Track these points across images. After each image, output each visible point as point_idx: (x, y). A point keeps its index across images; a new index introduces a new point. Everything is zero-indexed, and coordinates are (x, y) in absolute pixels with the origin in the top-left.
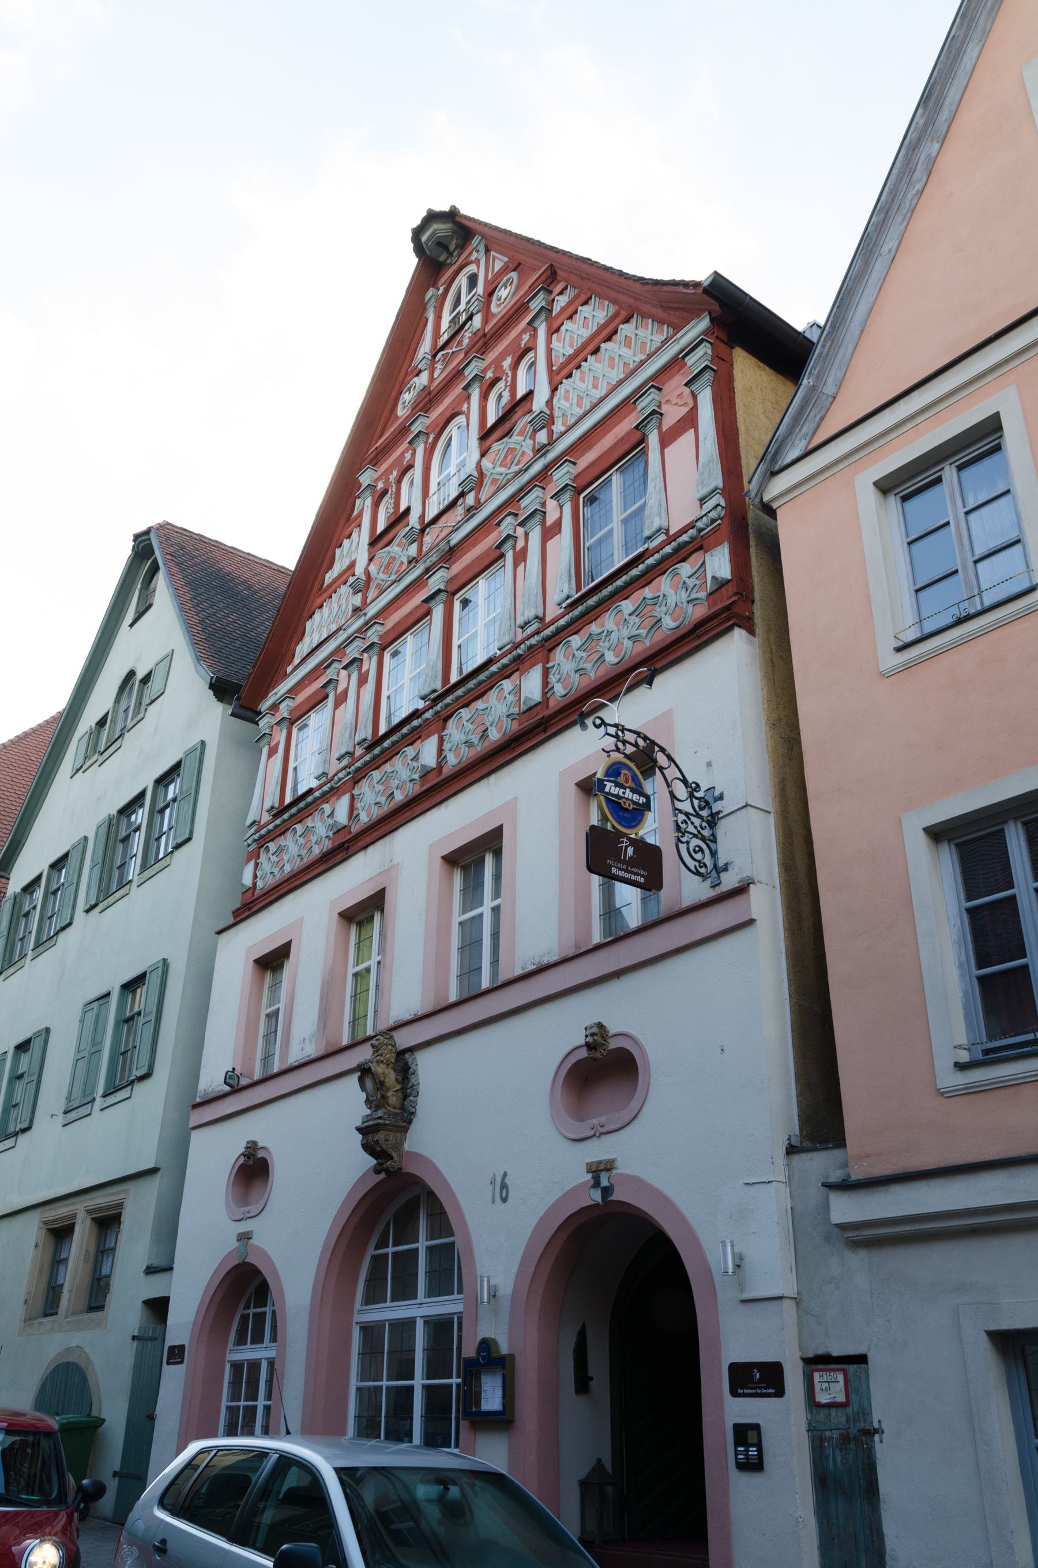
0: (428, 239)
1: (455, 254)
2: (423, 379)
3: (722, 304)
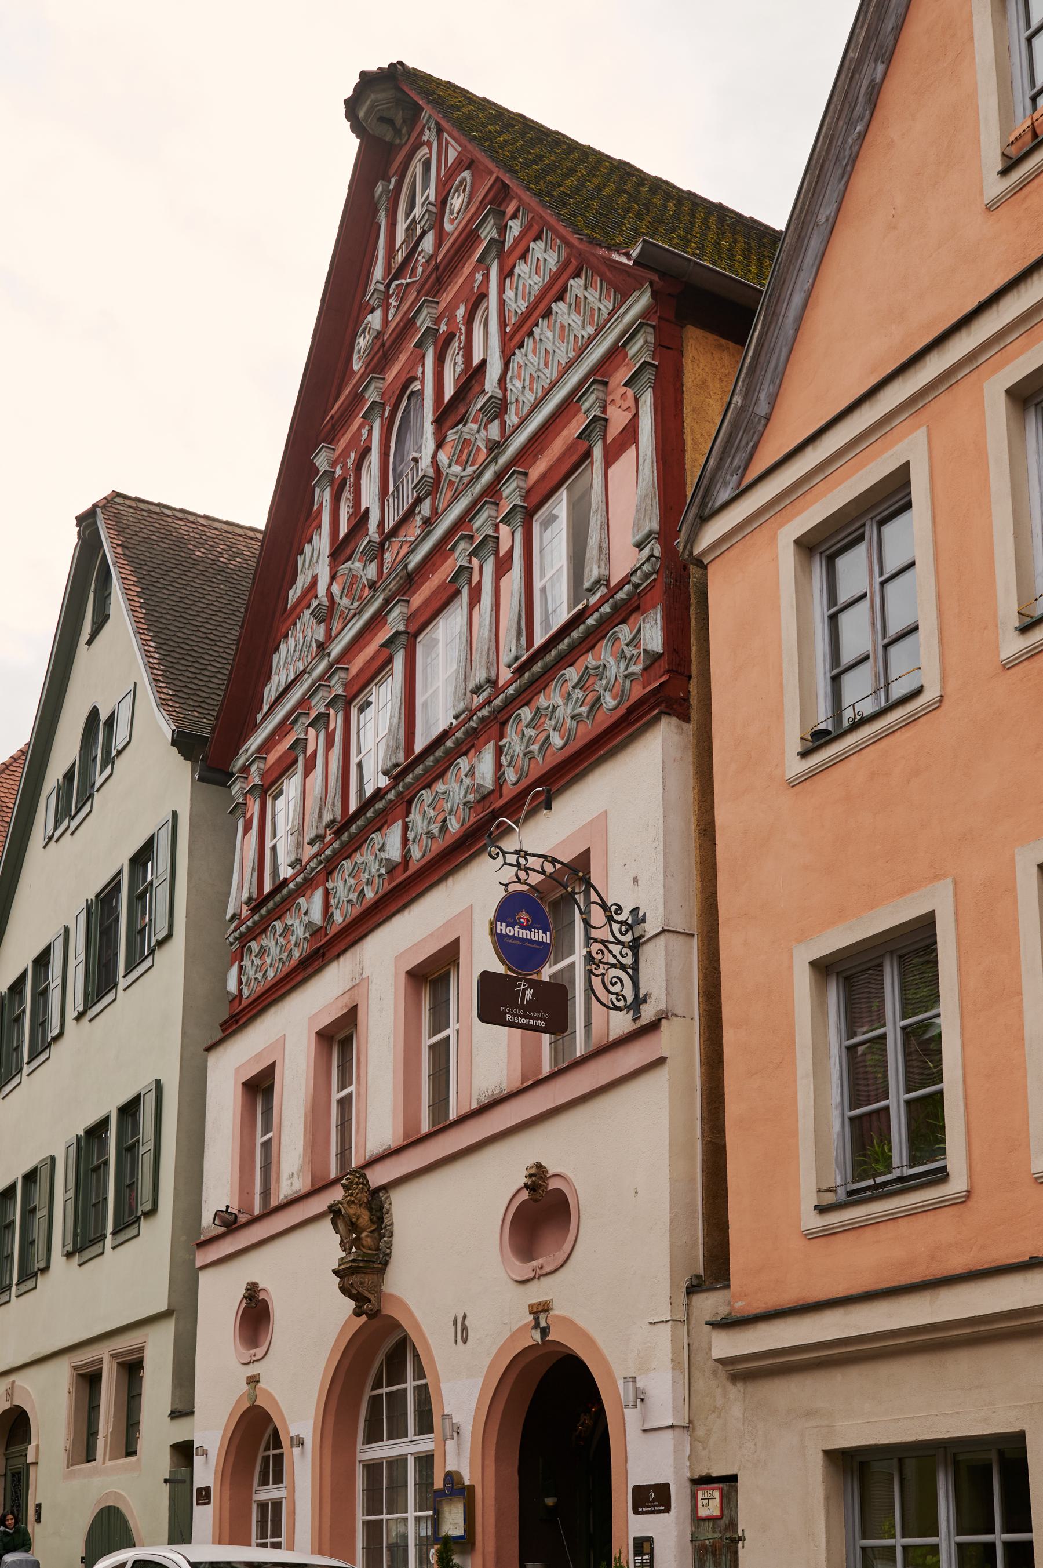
0: (368, 113)
1: (404, 131)
2: (375, 320)
3: (663, 274)
